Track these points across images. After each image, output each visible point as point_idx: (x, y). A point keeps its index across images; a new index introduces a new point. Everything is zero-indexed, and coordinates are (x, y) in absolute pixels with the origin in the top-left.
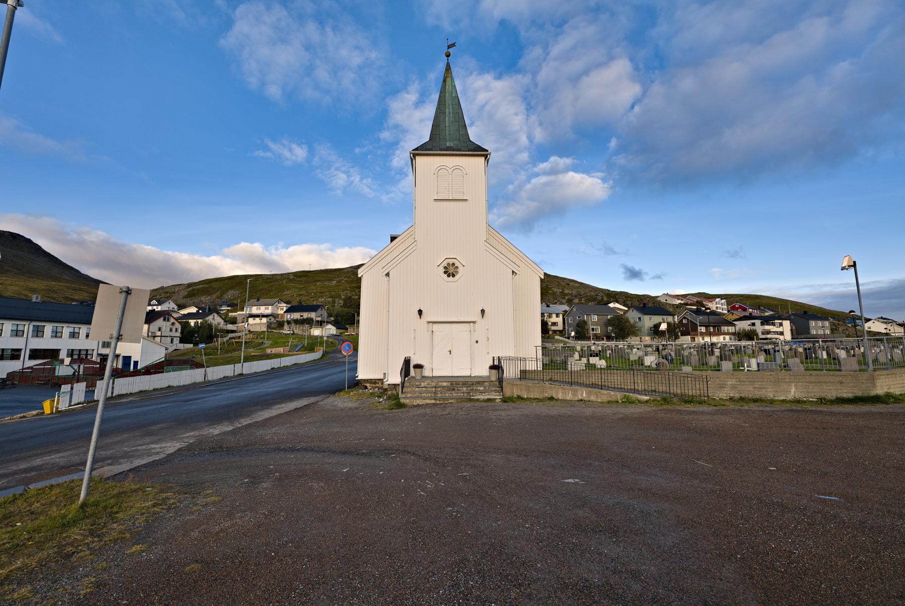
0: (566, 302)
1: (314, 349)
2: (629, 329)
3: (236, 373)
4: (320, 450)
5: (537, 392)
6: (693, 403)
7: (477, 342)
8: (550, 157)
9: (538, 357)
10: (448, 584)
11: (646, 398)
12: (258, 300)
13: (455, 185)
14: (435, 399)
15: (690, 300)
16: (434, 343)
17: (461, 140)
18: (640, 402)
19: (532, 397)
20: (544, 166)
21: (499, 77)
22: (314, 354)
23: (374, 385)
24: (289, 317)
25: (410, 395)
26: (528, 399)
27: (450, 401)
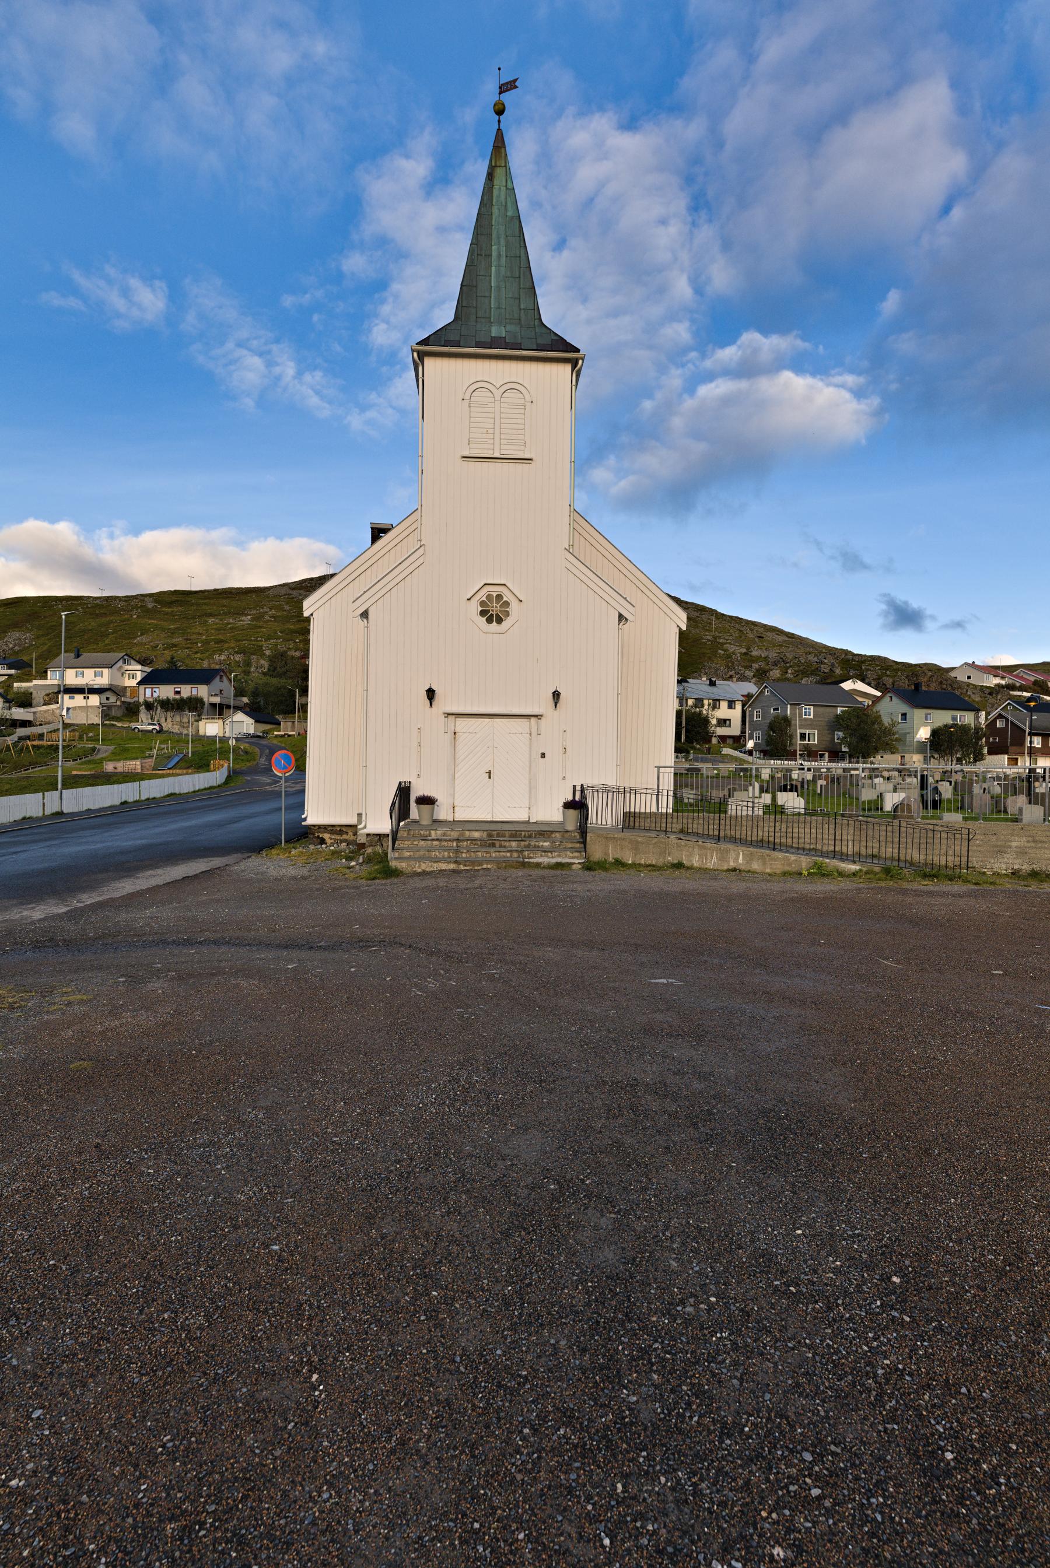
0: (754, 676)
1: (208, 765)
2: (880, 738)
3: (48, 812)
4: (240, 943)
5: (653, 853)
6: (937, 878)
7: (543, 755)
8: (742, 334)
9: (661, 787)
10: (444, 1079)
11: (854, 867)
12: (78, 656)
13: (507, 431)
14: (456, 862)
15: (1022, 678)
16: (457, 756)
17: (523, 322)
18: (841, 874)
19: (643, 862)
20: (729, 354)
21: (630, 125)
22: (208, 773)
23: (338, 837)
24: (148, 693)
25: (408, 854)
26: (634, 866)
27: (485, 866)
